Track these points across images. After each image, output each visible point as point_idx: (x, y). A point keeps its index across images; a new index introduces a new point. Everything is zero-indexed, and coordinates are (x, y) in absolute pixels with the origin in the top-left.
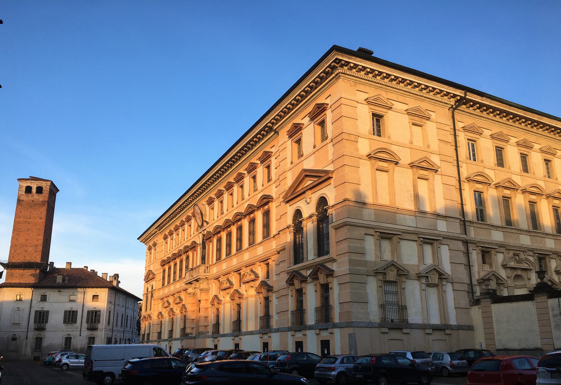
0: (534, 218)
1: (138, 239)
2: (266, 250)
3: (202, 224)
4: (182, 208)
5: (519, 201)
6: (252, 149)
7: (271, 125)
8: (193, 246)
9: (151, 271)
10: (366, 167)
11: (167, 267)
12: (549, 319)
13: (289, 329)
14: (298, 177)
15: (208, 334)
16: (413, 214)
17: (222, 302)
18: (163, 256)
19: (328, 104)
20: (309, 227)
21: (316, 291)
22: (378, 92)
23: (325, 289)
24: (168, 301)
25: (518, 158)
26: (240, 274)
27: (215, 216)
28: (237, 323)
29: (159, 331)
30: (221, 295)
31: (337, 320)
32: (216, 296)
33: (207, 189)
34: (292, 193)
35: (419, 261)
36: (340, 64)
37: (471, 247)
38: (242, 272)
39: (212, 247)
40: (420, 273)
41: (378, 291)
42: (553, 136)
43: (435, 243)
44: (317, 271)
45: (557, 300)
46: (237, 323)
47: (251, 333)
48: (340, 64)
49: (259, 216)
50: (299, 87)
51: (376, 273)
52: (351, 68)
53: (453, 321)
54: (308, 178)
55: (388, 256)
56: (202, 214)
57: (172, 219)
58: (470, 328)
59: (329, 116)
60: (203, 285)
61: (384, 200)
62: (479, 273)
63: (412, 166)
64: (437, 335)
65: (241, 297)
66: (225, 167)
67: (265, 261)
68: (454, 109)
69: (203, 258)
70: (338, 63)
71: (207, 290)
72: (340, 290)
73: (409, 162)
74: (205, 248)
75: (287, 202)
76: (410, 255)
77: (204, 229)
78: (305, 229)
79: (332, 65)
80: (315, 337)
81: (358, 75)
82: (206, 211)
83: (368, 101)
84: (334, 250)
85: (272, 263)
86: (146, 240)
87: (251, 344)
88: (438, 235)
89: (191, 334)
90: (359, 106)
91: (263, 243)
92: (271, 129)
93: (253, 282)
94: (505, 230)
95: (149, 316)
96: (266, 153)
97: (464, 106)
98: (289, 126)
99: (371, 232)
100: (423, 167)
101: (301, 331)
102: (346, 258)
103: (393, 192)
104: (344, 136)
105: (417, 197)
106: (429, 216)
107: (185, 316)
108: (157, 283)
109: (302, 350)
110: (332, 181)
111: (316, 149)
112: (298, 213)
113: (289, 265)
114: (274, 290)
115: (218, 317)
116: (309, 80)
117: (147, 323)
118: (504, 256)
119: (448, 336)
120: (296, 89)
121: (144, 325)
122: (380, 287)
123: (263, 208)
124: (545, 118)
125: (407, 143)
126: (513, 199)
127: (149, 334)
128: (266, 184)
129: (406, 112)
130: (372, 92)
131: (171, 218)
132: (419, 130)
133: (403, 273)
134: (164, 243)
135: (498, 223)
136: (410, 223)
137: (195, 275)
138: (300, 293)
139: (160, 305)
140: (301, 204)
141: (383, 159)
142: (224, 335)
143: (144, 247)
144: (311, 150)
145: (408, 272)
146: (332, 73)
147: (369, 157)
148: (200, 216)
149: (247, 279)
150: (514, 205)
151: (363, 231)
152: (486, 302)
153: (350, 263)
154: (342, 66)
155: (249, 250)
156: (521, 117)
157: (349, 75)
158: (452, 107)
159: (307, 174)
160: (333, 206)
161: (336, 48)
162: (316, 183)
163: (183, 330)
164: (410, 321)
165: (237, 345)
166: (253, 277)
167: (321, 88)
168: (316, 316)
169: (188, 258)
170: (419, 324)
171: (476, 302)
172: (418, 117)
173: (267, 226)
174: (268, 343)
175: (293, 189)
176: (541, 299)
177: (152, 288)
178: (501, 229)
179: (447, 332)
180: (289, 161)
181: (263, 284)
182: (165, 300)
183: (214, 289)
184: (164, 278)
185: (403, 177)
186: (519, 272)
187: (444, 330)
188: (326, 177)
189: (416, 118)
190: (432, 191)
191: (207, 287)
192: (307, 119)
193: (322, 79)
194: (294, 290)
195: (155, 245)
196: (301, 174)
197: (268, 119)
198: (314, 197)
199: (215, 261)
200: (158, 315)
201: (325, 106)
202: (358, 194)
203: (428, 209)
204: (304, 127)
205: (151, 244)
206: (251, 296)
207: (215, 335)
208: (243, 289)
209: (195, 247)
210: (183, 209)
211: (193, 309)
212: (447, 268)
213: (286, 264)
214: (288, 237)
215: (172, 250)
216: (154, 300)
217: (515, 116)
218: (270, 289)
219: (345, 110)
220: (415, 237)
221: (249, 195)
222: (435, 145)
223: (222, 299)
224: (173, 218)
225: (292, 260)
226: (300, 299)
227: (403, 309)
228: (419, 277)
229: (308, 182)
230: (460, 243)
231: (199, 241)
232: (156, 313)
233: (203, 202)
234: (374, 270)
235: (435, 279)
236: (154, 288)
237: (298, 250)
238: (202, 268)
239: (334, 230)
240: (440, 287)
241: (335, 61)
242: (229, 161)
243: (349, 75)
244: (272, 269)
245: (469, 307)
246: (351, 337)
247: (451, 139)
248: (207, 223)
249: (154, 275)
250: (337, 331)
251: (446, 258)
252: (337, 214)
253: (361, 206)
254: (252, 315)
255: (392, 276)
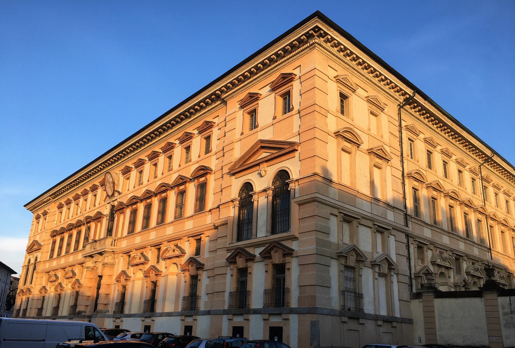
0: (451, 220)
1: (25, 206)
2: (200, 223)
3: (113, 195)
4: (88, 176)
5: (443, 203)
6: (190, 117)
7: (220, 93)
8: (98, 217)
9: (37, 242)
10: (333, 146)
11: (58, 239)
12: (499, 318)
13: (225, 312)
14: (252, 148)
15: (107, 313)
16: (369, 200)
17: (132, 279)
18: (55, 225)
19: (296, 75)
20: (262, 202)
21: (266, 271)
22: (347, 73)
23: (280, 271)
24: (55, 275)
25: (441, 163)
26: (129, 256)
27: (129, 187)
28: (151, 304)
29: (40, 307)
30: (131, 272)
31: (294, 303)
32: (124, 272)
33: (124, 157)
34: (241, 165)
35: (373, 248)
36: (318, 34)
37: (411, 240)
38: (132, 254)
39: (123, 221)
40: (375, 261)
41: (339, 276)
42: (465, 150)
43: (386, 233)
44: (272, 249)
45: (508, 298)
46: (151, 304)
47: (169, 315)
48: (318, 34)
49: (191, 189)
50: (264, 53)
51: (340, 256)
52: (328, 41)
53: (397, 315)
54: (264, 150)
55: (347, 240)
56: (114, 183)
57: (72, 187)
58: (410, 321)
59: (296, 87)
60: (108, 259)
61: (346, 181)
62: (415, 266)
63: (370, 152)
64: (386, 328)
65: (158, 273)
66: (152, 135)
67: (197, 238)
68: (401, 107)
69: (110, 231)
70: (316, 32)
71: (113, 265)
72: (301, 272)
73: (367, 148)
74: (113, 220)
75: (234, 174)
76: (366, 241)
77: (114, 199)
78: (255, 203)
79: (310, 32)
80: (262, 323)
81: (331, 49)
82: (119, 180)
83: (337, 79)
84: (295, 227)
85: (205, 239)
86: (35, 208)
87: (160, 326)
88: (389, 225)
89: (85, 312)
90: (329, 81)
91: (194, 217)
92: (218, 97)
93: (177, 259)
94: (433, 228)
95: (29, 290)
96: (207, 123)
97: (408, 106)
98: (243, 95)
99: (336, 212)
100: (379, 155)
101: (242, 315)
102: (313, 237)
103: (354, 175)
104: (317, 108)
105: (372, 184)
106: (381, 205)
107: (77, 293)
108: (42, 255)
109: (191, 334)
110: (297, 154)
111: (276, 121)
112: (248, 187)
113: (229, 240)
114: (206, 268)
115: (123, 295)
116: (278, 47)
117: (24, 298)
118: (433, 254)
119: (394, 329)
120: (260, 56)
121: (20, 300)
122: (342, 271)
123: (178, 188)
124: (464, 132)
125: (366, 129)
126: (438, 200)
127: (25, 310)
128: (203, 156)
129: (366, 99)
130: (341, 72)
131: (71, 186)
132: (377, 118)
133: (360, 258)
134: (57, 212)
135: (428, 221)
136: (366, 208)
137: (99, 247)
138: (243, 274)
139: (44, 279)
140: (252, 177)
141: (348, 138)
142: (130, 316)
143: (32, 216)
144: (270, 120)
145: (366, 259)
146: (307, 43)
147: (337, 134)
148: (112, 185)
149: (137, 261)
150: (439, 207)
151: (329, 210)
152: (428, 296)
153: (317, 243)
154: (320, 36)
155: (174, 223)
156: (449, 127)
157: (323, 47)
158: (399, 105)
159: (264, 145)
160: (297, 180)
161: (318, 15)
162: (273, 156)
163: (75, 306)
164: (366, 311)
165: (147, 328)
166: (177, 253)
167: (290, 58)
168: (265, 300)
169: (89, 228)
170: (371, 315)
171: (417, 296)
172: (376, 107)
173: (201, 200)
174: (243, 327)
175: (243, 161)
176: (490, 296)
177: (36, 260)
178: (430, 227)
179: (394, 324)
180: (238, 131)
181: (192, 261)
182: (68, 269)
183: (121, 264)
184: (53, 250)
185: (363, 161)
186: (443, 270)
187: (391, 322)
188: (291, 149)
189: (374, 107)
190: (384, 180)
191: (112, 261)
192: (268, 88)
193: (293, 47)
194: (235, 270)
195: (45, 214)
196: (256, 144)
197: (218, 86)
198: (271, 171)
199: (125, 233)
200: (41, 289)
201: (293, 76)
202: (325, 170)
203: (379, 196)
204: (261, 97)
205: (40, 212)
206: (172, 274)
207: (118, 315)
208: (162, 266)
209: (100, 217)
210: (88, 177)
211: (90, 285)
212: (394, 258)
213: (228, 240)
214: (232, 212)
215: (66, 220)
216: (38, 273)
217: (445, 124)
218: (200, 267)
219: (318, 82)
220: (370, 224)
221: (162, 174)
222: (387, 138)
223: (132, 275)
224: (74, 185)
225: (269, 229)
226: (243, 279)
227: (359, 297)
228: (374, 265)
229: (264, 154)
230: (403, 236)
231: (106, 211)
232: (38, 287)
233: (116, 172)
234: (337, 253)
235: (385, 269)
236: (38, 260)
237: (244, 224)
238: (109, 240)
239: (297, 206)
240: (389, 276)
241: (313, 28)
242: (159, 128)
243: (323, 47)
244: (204, 245)
245: (409, 300)
246: (314, 325)
247: (397, 134)
248: (120, 193)
249: (40, 246)
250: (294, 319)
251: (394, 247)
252: (300, 190)
253: (328, 183)
254: (171, 294)
255: (352, 260)
